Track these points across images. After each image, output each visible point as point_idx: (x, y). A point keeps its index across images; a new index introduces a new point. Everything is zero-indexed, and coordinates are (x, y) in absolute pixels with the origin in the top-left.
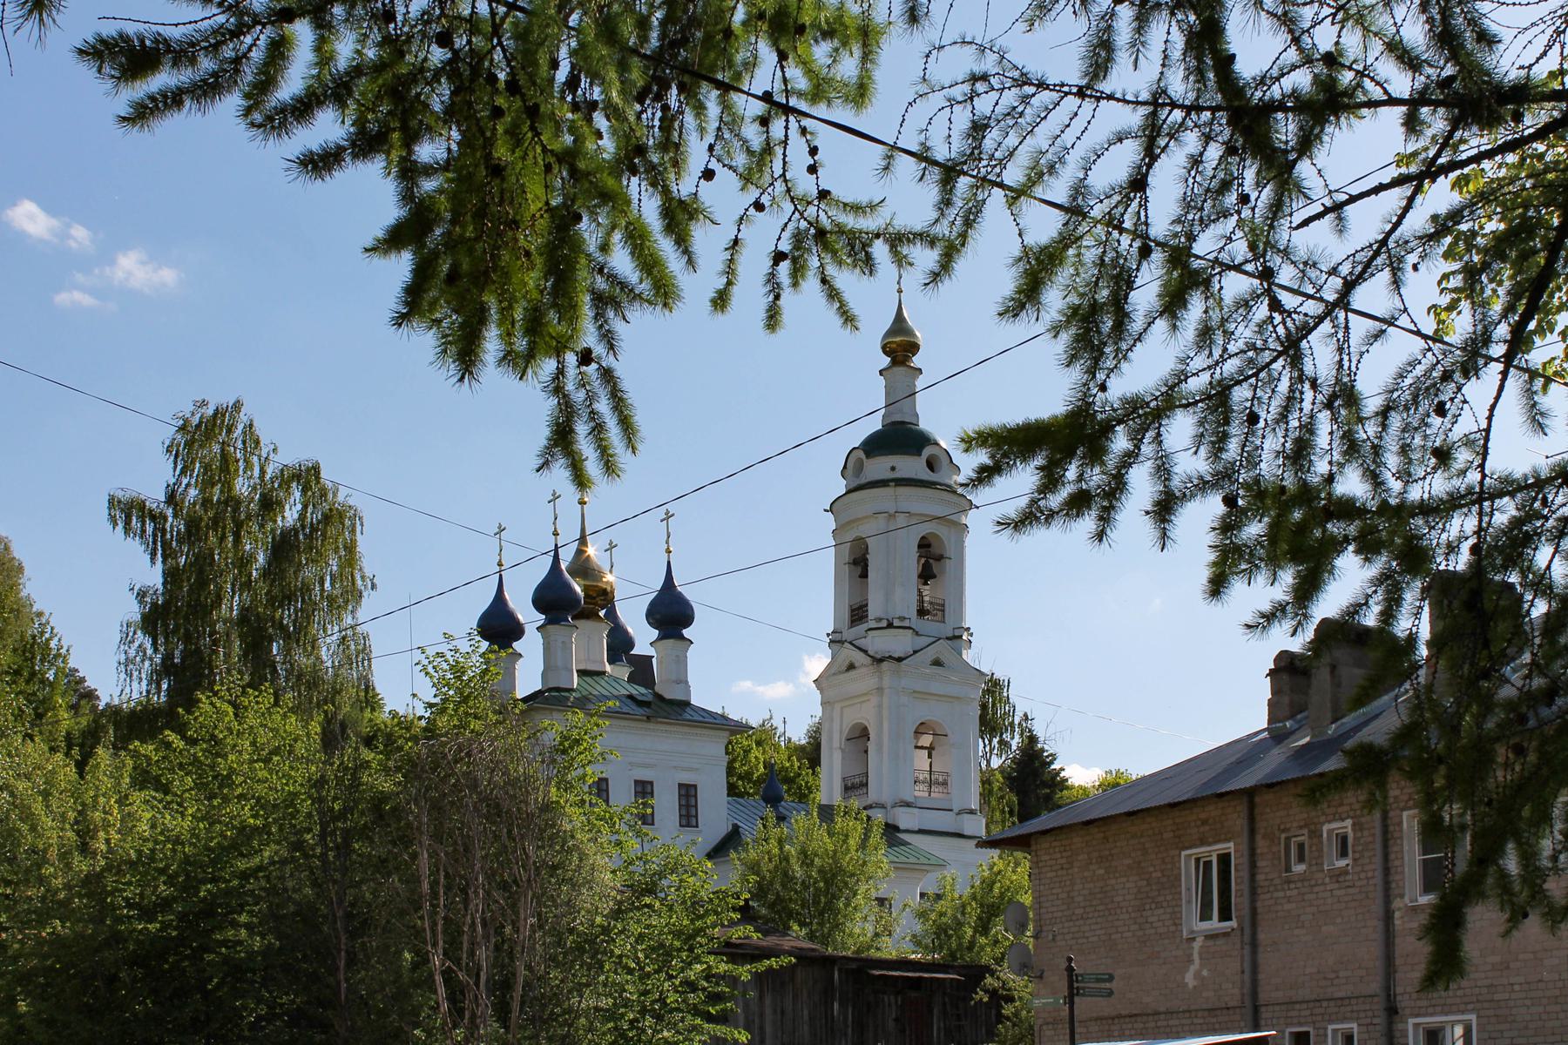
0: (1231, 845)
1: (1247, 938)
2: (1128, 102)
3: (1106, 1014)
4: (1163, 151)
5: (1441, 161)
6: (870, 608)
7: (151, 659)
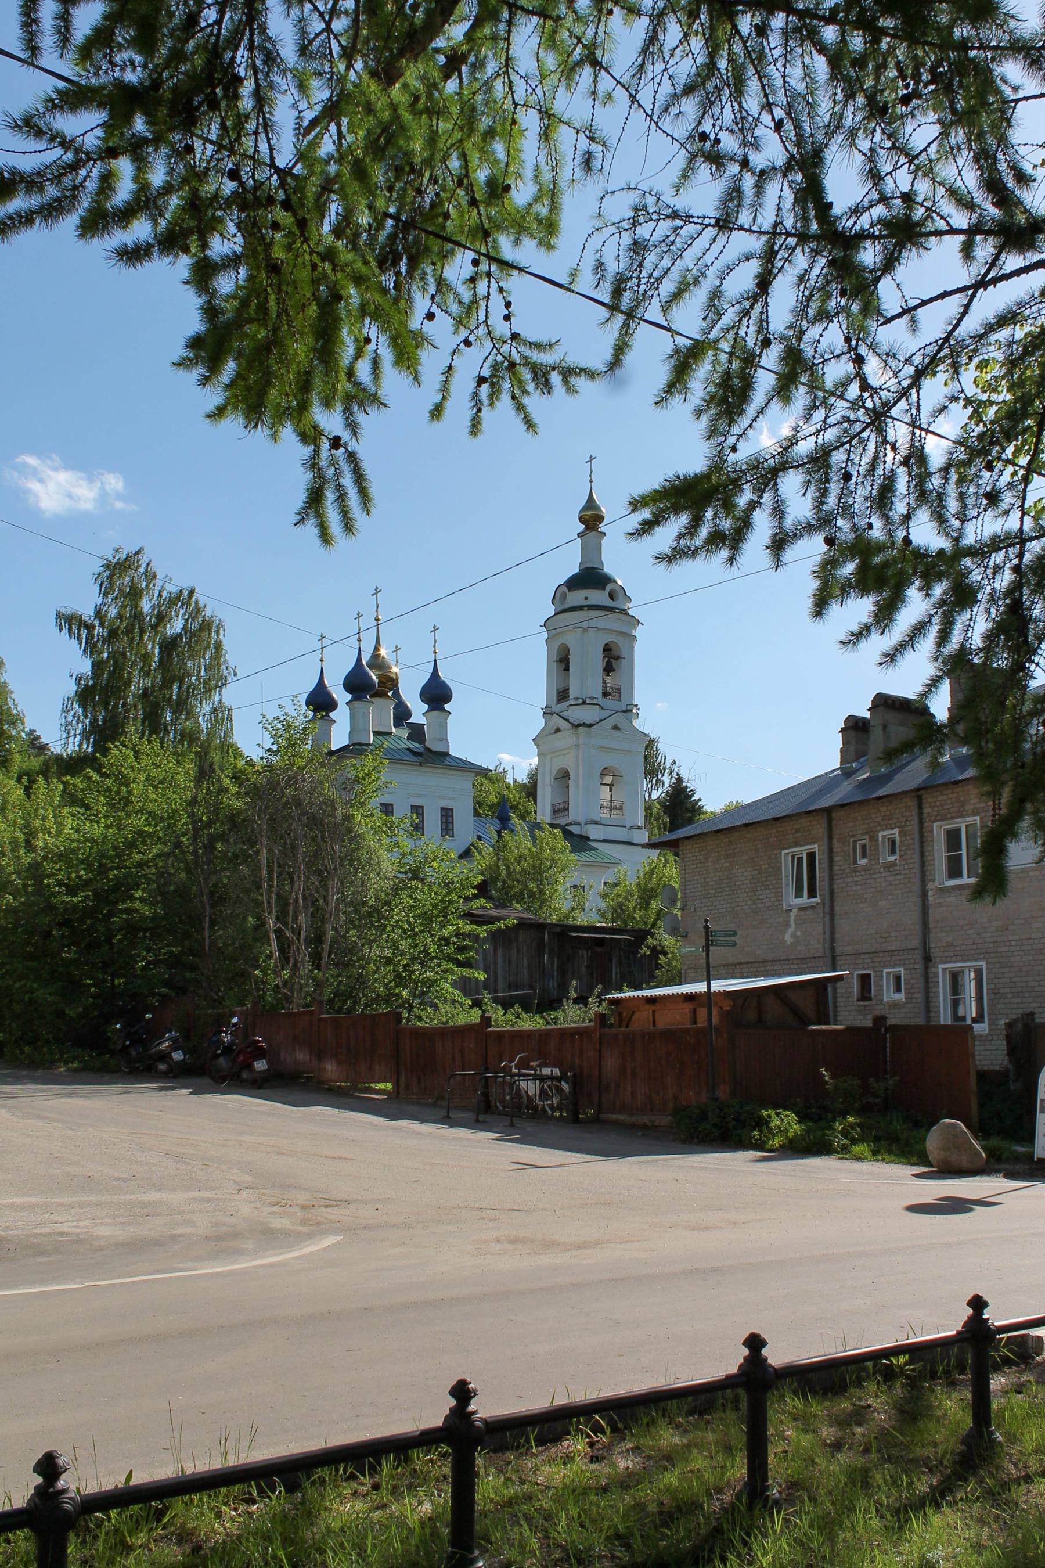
0: (816, 846)
1: (827, 909)
2: (754, 232)
3: (731, 962)
4: (779, 271)
5: (989, 277)
6: (570, 691)
7: (83, 722)
